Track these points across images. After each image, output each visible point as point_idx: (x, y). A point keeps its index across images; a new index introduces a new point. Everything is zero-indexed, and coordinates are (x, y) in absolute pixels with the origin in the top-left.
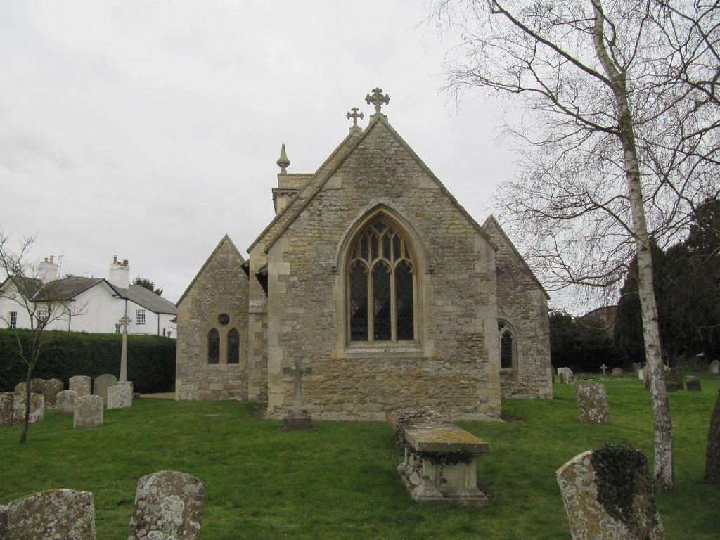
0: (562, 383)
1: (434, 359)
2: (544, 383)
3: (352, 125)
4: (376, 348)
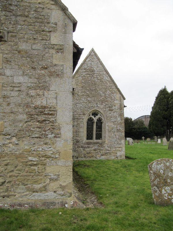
0: (129, 144)
2: (120, 149)
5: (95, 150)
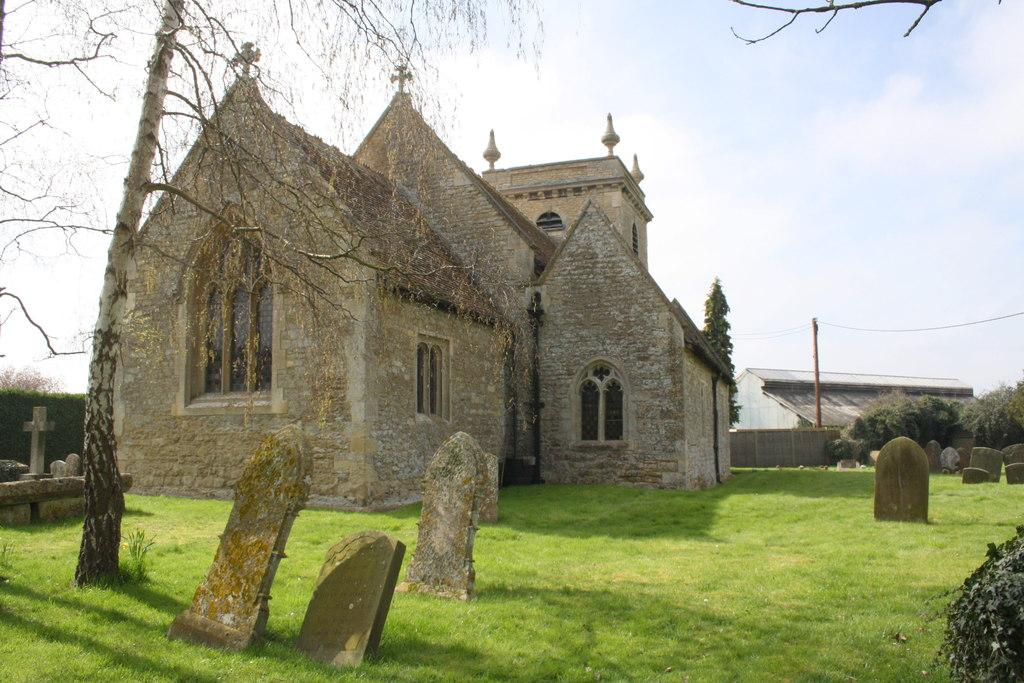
1: (282, 416)
3: (397, 89)
4: (220, 401)
5: (601, 466)
